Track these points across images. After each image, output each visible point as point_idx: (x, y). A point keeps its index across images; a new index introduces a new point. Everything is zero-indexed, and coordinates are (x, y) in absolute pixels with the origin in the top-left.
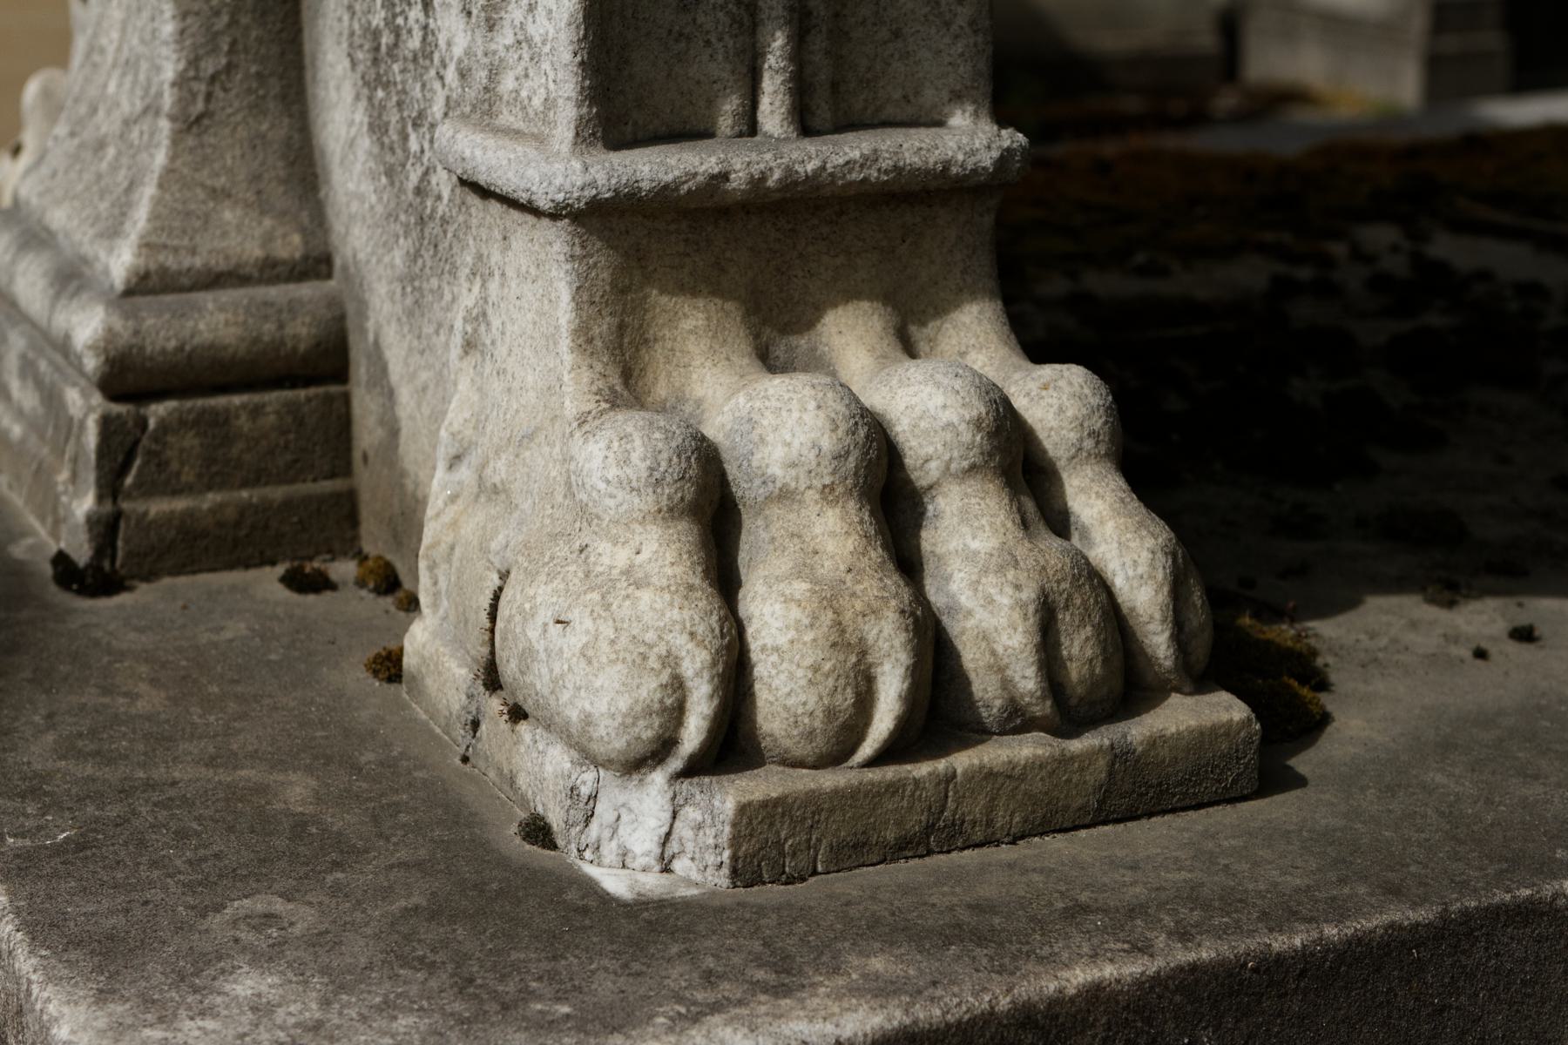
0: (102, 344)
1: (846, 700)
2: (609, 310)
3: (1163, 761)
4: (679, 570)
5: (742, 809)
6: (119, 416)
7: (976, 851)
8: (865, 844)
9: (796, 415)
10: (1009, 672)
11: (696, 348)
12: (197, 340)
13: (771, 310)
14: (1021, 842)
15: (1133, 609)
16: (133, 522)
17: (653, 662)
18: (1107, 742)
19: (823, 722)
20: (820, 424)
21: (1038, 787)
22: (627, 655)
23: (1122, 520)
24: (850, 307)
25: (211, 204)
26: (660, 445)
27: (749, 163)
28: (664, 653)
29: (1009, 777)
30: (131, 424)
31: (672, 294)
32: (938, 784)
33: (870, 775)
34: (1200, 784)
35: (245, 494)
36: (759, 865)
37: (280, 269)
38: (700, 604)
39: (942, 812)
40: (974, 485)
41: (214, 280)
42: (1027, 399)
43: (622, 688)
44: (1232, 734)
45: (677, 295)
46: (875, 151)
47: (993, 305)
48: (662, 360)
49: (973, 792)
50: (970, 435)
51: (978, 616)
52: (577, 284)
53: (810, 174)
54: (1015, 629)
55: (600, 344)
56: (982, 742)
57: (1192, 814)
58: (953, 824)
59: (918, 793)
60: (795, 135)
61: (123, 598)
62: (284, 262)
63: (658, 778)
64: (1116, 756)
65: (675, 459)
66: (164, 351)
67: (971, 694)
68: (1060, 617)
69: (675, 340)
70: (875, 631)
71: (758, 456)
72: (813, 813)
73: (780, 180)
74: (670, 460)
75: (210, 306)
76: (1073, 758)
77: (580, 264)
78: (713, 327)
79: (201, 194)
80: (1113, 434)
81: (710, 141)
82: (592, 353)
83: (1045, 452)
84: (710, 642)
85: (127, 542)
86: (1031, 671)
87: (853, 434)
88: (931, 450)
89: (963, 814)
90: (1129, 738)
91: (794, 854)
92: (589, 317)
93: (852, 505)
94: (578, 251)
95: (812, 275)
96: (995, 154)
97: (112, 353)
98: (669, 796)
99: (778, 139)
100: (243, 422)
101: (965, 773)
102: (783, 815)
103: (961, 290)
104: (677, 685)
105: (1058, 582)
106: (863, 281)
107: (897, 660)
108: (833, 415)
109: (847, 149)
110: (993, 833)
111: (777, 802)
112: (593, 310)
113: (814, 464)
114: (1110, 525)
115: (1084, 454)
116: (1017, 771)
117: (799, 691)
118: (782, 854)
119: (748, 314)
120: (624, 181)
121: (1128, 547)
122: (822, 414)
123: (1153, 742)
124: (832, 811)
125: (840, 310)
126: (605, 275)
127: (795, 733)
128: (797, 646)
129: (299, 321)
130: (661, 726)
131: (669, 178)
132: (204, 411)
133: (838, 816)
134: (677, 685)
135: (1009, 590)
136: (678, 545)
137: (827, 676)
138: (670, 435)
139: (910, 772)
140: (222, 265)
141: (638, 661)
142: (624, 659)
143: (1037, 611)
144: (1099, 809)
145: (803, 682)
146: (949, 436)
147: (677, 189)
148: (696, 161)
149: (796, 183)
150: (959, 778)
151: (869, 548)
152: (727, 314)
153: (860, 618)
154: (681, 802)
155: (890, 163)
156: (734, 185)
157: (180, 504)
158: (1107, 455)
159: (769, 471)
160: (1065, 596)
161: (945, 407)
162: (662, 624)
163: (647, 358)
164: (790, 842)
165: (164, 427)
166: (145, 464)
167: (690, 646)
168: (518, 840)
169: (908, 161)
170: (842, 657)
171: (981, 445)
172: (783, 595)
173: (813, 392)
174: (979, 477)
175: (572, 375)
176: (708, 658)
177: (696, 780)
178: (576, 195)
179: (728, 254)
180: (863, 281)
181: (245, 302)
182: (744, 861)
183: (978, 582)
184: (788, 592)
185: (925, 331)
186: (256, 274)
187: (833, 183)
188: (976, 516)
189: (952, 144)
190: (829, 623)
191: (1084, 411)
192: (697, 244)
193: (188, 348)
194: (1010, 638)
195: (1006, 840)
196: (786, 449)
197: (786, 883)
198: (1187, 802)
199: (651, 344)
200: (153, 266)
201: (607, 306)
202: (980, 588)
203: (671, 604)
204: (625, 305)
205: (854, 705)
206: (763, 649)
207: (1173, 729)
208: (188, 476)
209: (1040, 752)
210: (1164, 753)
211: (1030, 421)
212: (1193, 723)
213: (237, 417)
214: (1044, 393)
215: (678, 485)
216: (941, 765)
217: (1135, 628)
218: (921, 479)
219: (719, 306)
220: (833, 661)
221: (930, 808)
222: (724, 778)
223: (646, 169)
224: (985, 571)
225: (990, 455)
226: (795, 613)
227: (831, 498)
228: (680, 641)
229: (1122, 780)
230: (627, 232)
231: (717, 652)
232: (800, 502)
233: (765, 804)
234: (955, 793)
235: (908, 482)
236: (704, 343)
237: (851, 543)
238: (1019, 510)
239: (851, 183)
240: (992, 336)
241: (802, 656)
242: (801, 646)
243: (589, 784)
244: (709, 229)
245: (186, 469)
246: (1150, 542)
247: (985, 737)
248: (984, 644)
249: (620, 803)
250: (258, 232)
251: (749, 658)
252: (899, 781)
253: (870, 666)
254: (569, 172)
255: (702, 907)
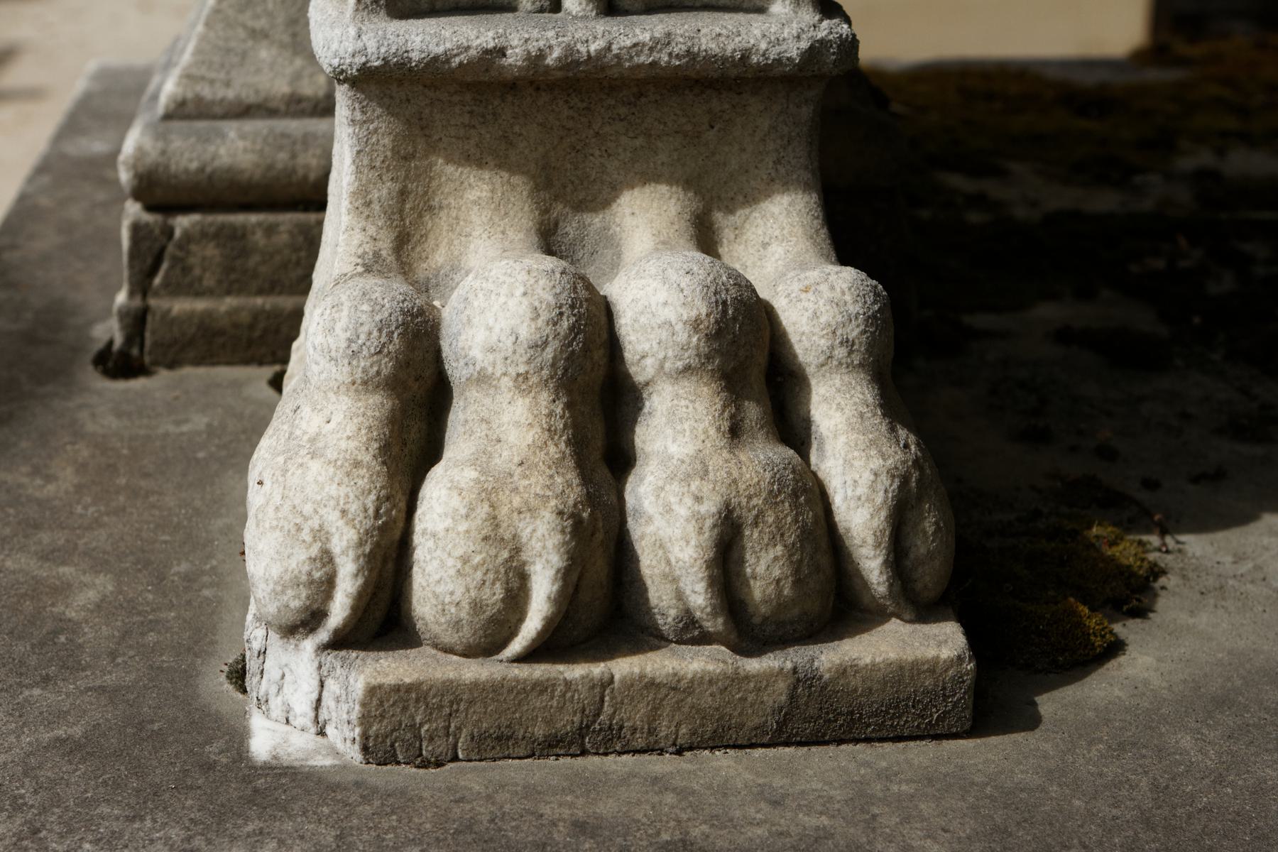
0: (131, 161)
1: (495, 595)
2: (390, 175)
3: (855, 690)
4: (352, 444)
5: (372, 691)
6: (147, 225)
7: (637, 756)
8: (509, 738)
9: (502, 299)
10: (681, 585)
11: (478, 219)
12: (217, 163)
13: (565, 187)
14: (688, 754)
15: (848, 530)
16: (158, 317)
17: (306, 535)
18: (789, 665)
19: (469, 614)
20: (521, 312)
21: (707, 701)
22: (286, 524)
23: (855, 435)
24: (648, 189)
25: (250, 43)
26: (364, 318)
27: (527, 40)
28: (317, 527)
29: (674, 689)
30: (157, 231)
31: (459, 164)
32: (593, 687)
33: (516, 671)
34: (900, 717)
35: (259, 301)
36: (392, 745)
37: (304, 105)
38: (360, 482)
39: (598, 715)
40: (687, 386)
41: (244, 111)
42: (787, 300)
43: (276, 556)
44: (938, 671)
45: (463, 166)
46: (669, 35)
47: (807, 198)
48: (445, 228)
49: (632, 699)
50: (686, 335)
51: (656, 523)
52: (358, 148)
53: (593, 54)
54: (688, 542)
55: (378, 208)
56: (658, 648)
57: (888, 746)
58: (610, 728)
59: (569, 695)
60: (594, 13)
61: (138, 384)
62: (308, 99)
63: (309, 645)
64: (798, 680)
65: (375, 333)
66: (186, 171)
67: (647, 599)
68: (747, 533)
69: (459, 209)
70: (529, 530)
71: (463, 337)
72: (452, 703)
73: (559, 59)
74: (370, 334)
75: (232, 134)
76: (747, 678)
77: (360, 128)
78: (496, 200)
79: (241, 33)
80: (871, 346)
81: (510, 15)
82: (368, 216)
83: (795, 356)
84: (361, 522)
85: (153, 333)
86: (701, 587)
87: (555, 324)
88: (646, 346)
89: (622, 719)
90: (816, 664)
91: (431, 739)
92: (369, 181)
93: (545, 397)
94: (358, 116)
95: (609, 155)
96: (804, 45)
97: (140, 170)
98: (316, 664)
99: (575, 17)
100: (259, 238)
101: (623, 680)
102: (417, 700)
103: (772, 180)
104: (325, 560)
105: (750, 498)
106: (663, 164)
107: (548, 561)
108: (537, 304)
109: (638, 31)
110: (656, 742)
111: (409, 688)
112: (373, 175)
113: (510, 350)
114: (843, 439)
115: (835, 363)
116: (683, 684)
117: (448, 580)
118: (418, 737)
119: (537, 188)
120: (393, 50)
121: (852, 465)
122: (525, 301)
123: (842, 671)
124: (471, 702)
125: (636, 192)
126: (387, 141)
127: (443, 620)
128: (452, 535)
129: (311, 152)
130: (308, 598)
131: (440, 50)
132: (222, 227)
133: (478, 707)
134: (327, 558)
135: (689, 501)
136: (361, 419)
137: (476, 569)
138: (378, 308)
139: (561, 673)
140: (252, 98)
141: (293, 532)
142: (283, 527)
143: (715, 526)
144: (780, 730)
145: (452, 572)
146: (664, 335)
147: (448, 61)
148: (472, 35)
149: (577, 63)
150: (616, 685)
151: (549, 443)
152: (513, 187)
153: (516, 514)
154: (325, 674)
155: (684, 48)
156: (511, 61)
157: (200, 305)
158: (861, 365)
159: (472, 354)
160: (755, 512)
161: (666, 304)
162: (319, 498)
163: (430, 225)
164: (426, 727)
165: (188, 237)
166: (171, 267)
167: (341, 523)
168: (223, 678)
169: (703, 47)
170: (493, 552)
171: (697, 347)
172: (452, 481)
173: (526, 277)
174: (694, 378)
175: (345, 236)
176: (355, 537)
177: (343, 653)
178: (348, 61)
179: (517, 129)
180: (663, 164)
181: (265, 132)
182: (375, 740)
183: (662, 488)
184: (457, 478)
185: (731, 218)
186: (283, 108)
187: (619, 64)
188: (681, 420)
189: (757, 32)
190: (484, 516)
191: (839, 318)
192: (483, 116)
193: (209, 169)
194: (681, 550)
195: (671, 750)
196: (488, 333)
197: (418, 767)
198: (884, 733)
199: (436, 211)
200: (190, 95)
201: (388, 170)
202: (662, 495)
203: (332, 479)
204: (408, 171)
205: (503, 600)
206: (424, 532)
207: (868, 660)
208: (209, 281)
209: (711, 667)
210: (856, 682)
211: (784, 323)
212: (892, 656)
213: (254, 233)
214: (803, 296)
215: (375, 358)
216: (597, 669)
217: (851, 549)
218: (639, 378)
219: (505, 179)
220: (484, 555)
221: (583, 710)
222: (373, 655)
223: (419, 39)
224: (672, 478)
225: (709, 357)
226: (456, 502)
227: (524, 387)
228: (332, 518)
229: (806, 704)
230: (408, 100)
231: (367, 532)
232: (496, 387)
233: (397, 689)
234: (612, 698)
235: (628, 376)
236: (487, 214)
237: (531, 436)
238: (732, 417)
239: (639, 66)
240: (799, 230)
241: (455, 546)
242: (454, 535)
243: (259, 640)
244: (496, 103)
245: (207, 275)
246: (876, 463)
247: (663, 643)
248: (660, 552)
249: (283, 663)
250: (289, 71)
251: (412, 540)
252: (548, 680)
253: (524, 563)
254: (344, 38)
255: (320, 781)
